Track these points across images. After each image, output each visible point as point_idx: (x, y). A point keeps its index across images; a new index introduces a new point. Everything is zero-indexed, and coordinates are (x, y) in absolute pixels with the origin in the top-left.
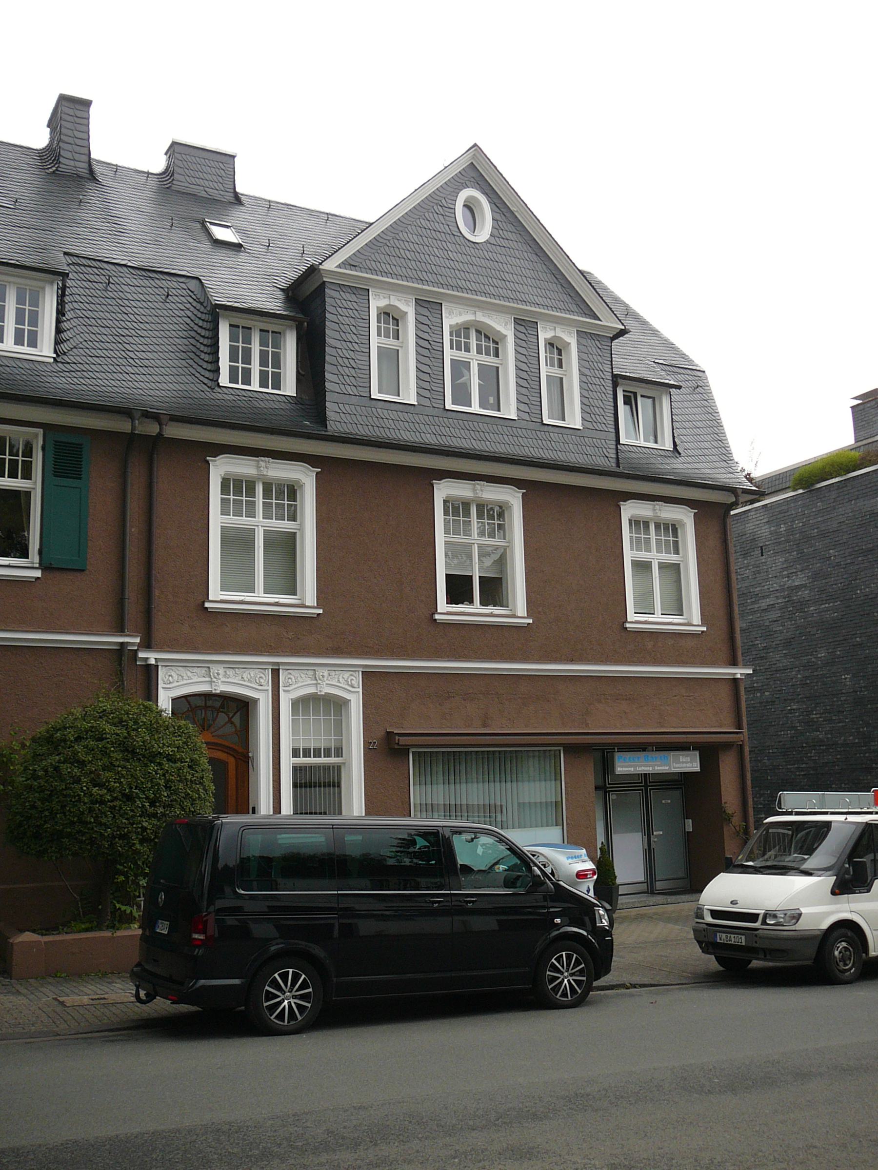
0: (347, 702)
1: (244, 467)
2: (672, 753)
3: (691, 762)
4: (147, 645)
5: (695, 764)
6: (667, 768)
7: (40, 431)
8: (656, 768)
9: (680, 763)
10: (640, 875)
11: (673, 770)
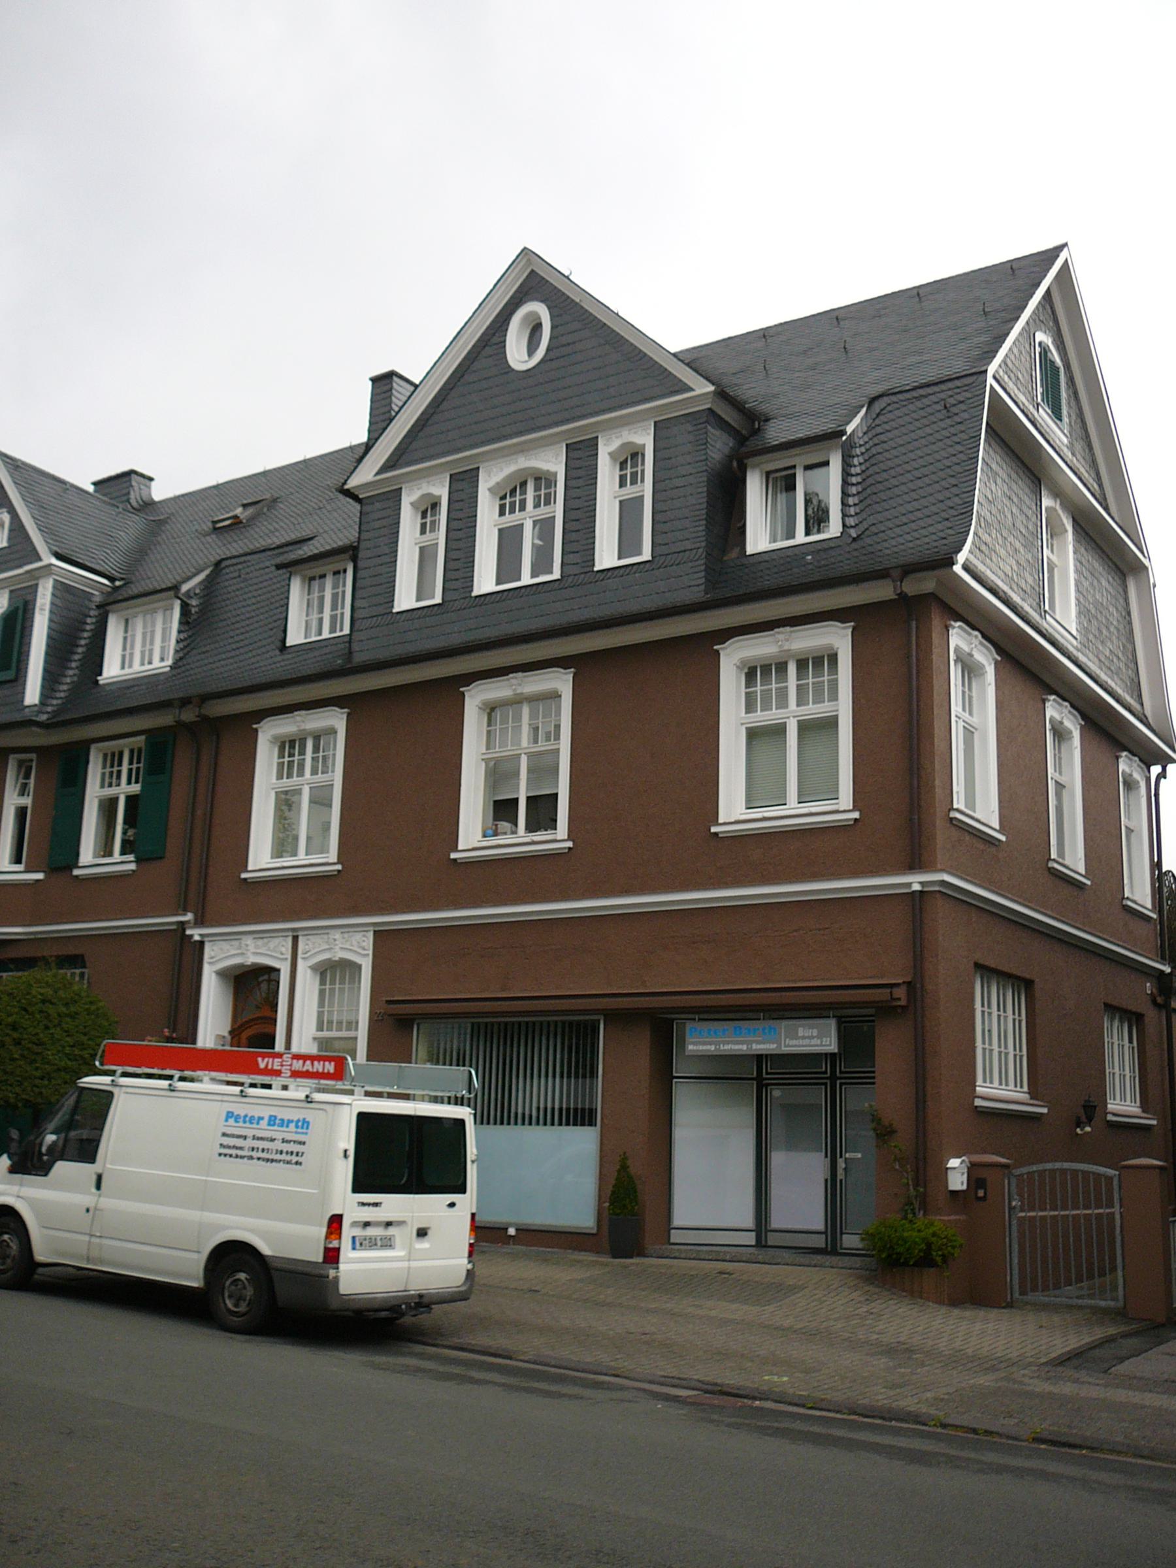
0: (278, 970)
1: (761, 647)
2: (784, 1023)
3: (817, 1037)
4: (200, 922)
5: (826, 1041)
6: (774, 1046)
7: (34, 756)
8: (754, 1046)
9: (797, 1038)
10: (815, 1219)
11: (785, 1050)
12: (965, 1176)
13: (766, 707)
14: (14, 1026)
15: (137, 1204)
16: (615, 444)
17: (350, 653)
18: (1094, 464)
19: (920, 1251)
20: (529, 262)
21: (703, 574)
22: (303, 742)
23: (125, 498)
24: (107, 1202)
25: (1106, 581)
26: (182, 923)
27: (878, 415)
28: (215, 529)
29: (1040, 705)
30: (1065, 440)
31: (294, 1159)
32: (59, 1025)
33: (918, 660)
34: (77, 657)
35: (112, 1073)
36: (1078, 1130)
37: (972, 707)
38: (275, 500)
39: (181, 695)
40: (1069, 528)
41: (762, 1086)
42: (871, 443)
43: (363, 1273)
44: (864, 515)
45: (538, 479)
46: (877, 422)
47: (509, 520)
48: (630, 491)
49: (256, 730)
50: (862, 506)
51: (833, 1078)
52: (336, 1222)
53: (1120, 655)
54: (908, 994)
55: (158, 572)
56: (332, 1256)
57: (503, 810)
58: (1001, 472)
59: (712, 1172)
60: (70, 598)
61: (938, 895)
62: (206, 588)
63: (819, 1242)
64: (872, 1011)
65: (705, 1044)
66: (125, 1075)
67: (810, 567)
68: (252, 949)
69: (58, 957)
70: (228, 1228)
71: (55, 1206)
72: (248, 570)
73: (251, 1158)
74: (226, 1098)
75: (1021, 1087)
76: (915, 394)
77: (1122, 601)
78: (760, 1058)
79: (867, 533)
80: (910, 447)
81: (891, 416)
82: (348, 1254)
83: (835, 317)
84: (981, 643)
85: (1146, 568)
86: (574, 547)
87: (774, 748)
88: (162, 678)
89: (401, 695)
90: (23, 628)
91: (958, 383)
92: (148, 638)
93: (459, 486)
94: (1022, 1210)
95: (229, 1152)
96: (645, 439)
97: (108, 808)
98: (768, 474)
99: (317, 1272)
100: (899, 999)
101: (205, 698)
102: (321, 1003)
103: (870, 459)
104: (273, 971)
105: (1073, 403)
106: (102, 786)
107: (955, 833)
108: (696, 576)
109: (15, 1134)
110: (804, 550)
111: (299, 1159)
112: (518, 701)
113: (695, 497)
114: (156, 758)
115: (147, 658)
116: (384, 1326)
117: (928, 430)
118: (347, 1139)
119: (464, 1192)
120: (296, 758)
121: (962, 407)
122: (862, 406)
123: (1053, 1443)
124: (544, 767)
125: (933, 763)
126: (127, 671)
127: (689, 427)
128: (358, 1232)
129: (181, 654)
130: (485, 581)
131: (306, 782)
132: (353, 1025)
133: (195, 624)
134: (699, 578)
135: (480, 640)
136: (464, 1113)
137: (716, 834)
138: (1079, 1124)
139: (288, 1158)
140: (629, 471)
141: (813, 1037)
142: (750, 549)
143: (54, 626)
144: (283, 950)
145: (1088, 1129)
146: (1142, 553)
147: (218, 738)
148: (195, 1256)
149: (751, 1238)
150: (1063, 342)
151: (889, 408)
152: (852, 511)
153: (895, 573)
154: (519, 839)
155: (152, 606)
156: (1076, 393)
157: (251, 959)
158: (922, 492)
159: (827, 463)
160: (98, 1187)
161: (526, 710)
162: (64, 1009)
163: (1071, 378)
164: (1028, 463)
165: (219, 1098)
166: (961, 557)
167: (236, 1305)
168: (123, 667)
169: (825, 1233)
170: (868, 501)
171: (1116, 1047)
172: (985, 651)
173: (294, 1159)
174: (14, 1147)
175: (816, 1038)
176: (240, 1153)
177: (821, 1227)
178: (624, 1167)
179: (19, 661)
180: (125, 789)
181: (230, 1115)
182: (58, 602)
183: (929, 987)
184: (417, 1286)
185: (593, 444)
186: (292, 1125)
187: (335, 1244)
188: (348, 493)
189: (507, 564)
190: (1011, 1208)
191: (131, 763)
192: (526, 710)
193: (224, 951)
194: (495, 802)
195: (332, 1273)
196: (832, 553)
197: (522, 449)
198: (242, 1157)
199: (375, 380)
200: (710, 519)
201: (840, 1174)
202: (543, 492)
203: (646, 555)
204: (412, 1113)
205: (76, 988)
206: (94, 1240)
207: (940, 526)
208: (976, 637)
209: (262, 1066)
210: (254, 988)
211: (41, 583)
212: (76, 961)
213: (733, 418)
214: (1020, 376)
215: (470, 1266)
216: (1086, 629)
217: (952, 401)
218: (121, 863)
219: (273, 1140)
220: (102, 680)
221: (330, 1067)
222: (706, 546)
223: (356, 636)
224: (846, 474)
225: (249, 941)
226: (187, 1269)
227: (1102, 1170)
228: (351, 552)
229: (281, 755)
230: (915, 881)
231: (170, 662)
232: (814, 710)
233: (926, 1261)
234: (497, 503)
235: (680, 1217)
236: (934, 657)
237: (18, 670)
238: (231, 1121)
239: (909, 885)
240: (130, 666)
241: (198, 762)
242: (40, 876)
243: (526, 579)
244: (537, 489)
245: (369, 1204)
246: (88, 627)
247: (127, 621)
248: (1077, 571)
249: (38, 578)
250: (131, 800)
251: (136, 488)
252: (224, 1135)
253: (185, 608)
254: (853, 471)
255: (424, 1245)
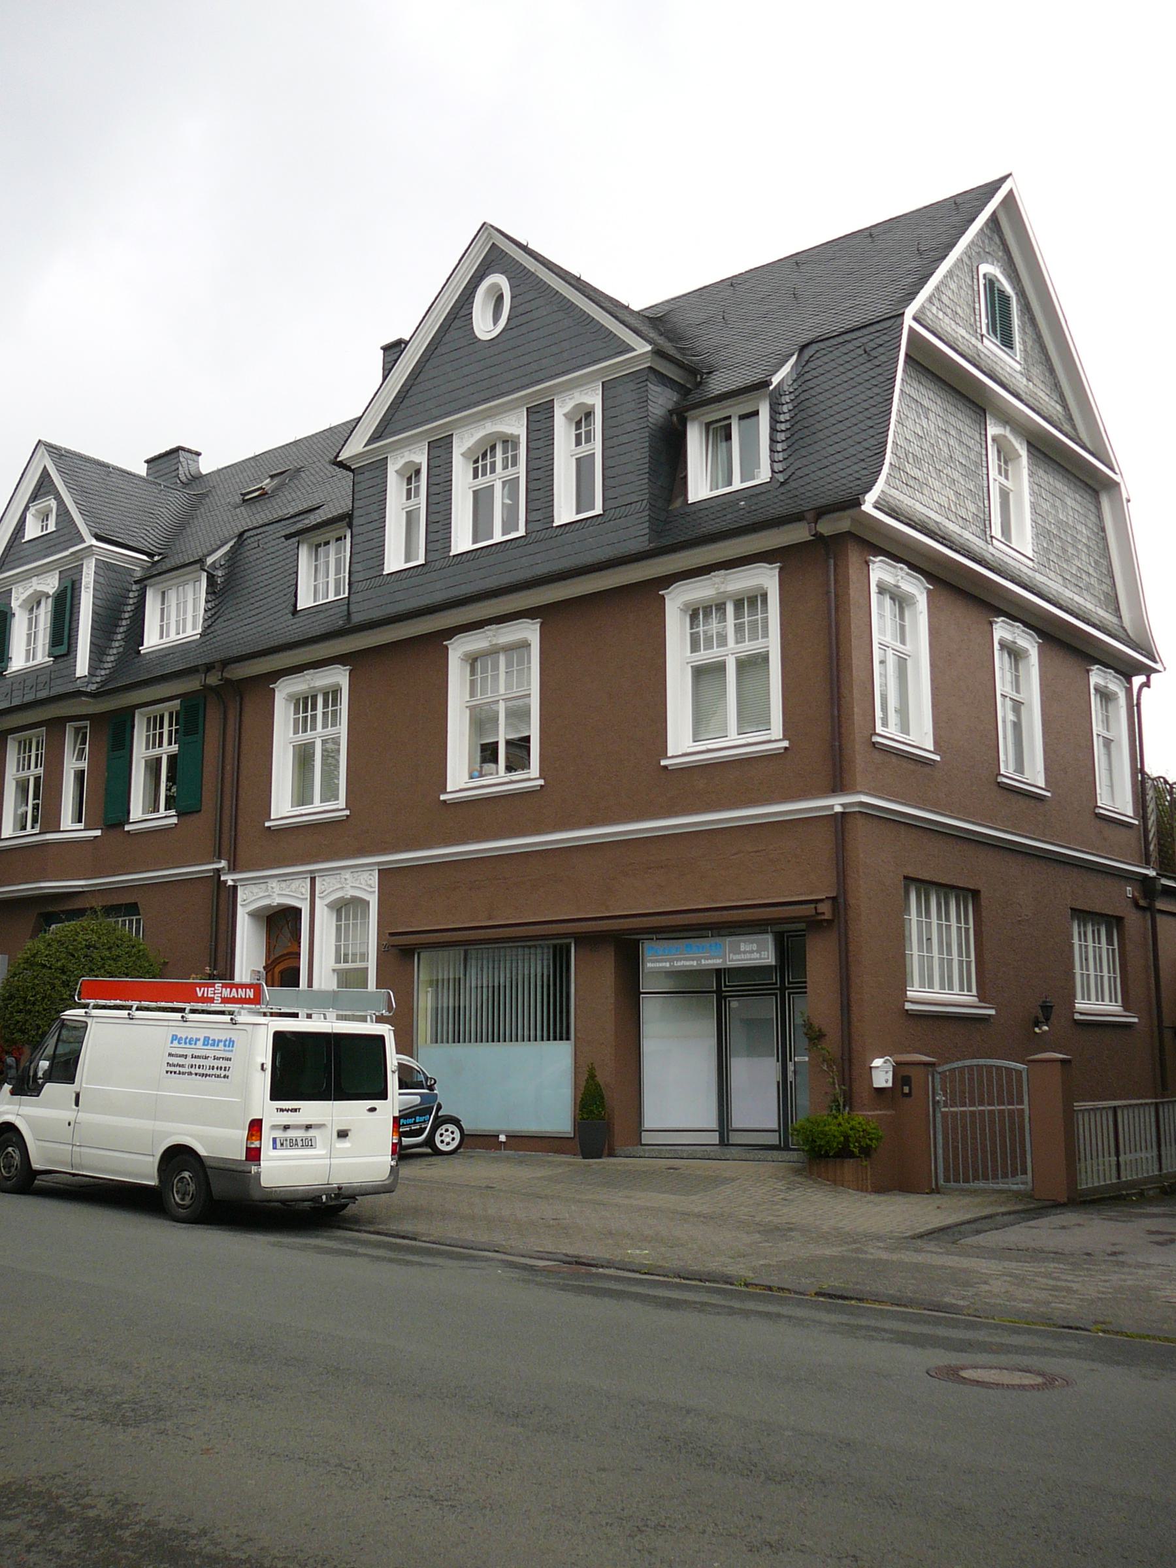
2: (728, 939)
3: (757, 951)
4: (233, 868)
5: (764, 954)
6: (719, 961)
8: (703, 962)
9: (740, 952)
11: (730, 964)
12: (891, 1073)
13: (709, 646)
14: (63, 971)
15: (115, 1118)
16: (568, 408)
17: (349, 614)
18: (1057, 386)
19: (839, 1143)
20: (490, 236)
21: (647, 524)
22: (314, 698)
23: (174, 474)
24: (84, 1116)
25: (1072, 502)
26: (218, 870)
27: (807, 362)
28: (244, 501)
29: (987, 627)
30: (1018, 367)
31: (223, 1073)
32: (103, 967)
33: (836, 595)
34: (122, 630)
35: (86, 1006)
36: (1037, 1030)
37: (899, 636)
38: (298, 470)
39: (207, 661)
40: (1023, 452)
41: (721, 998)
42: (800, 390)
43: (283, 1169)
44: (791, 460)
45: (505, 442)
46: (806, 369)
47: (482, 482)
48: (584, 449)
49: (273, 690)
50: (789, 452)
51: (783, 989)
52: (256, 1126)
53: (1091, 571)
54: (834, 910)
55: (191, 548)
56: (254, 1155)
57: (489, 753)
58: (933, 407)
59: (678, 1078)
60: (112, 575)
61: (858, 816)
62: (230, 559)
63: (773, 1139)
64: (802, 926)
65: (686, 959)
66: (96, 1007)
67: (742, 512)
68: (277, 891)
69: (104, 907)
70: (174, 1134)
71: (44, 1121)
72: (266, 540)
73: (190, 1074)
74: (171, 1023)
75: (970, 990)
76: (840, 340)
77: (1093, 518)
78: (718, 971)
79: (794, 477)
80: (834, 392)
81: (819, 363)
82: (267, 1152)
83: (796, 261)
84: (908, 574)
85: (1118, 484)
86: (537, 505)
87: (714, 684)
88: (193, 645)
89: (393, 651)
90: (72, 606)
91: (878, 327)
92: (181, 607)
93: (436, 452)
94: (945, 1106)
95: (174, 1070)
96: (594, 398)
97: (153, 766)
98: (708, 425)
99: (240, 1168)
100: (823, 914)
101: (225, 663)
102: (338, 939)
103: (799, 406)
104: (298, 911)
105: (1029, 330)
106: (147, 748)
107: (878, 757)
108: (641, 527)
109: (10, 1060)
110: (738, 496)
111: (227, 1073)
112: (494, 651)
113: (638, 454)
114: (189, 722)
115: (181, 626)
116: (319, 1214)
117: (850, 374)
118: (264, 1053)
119: (386, 1098)
120: (309, 713)
121: (881, 350)
122: (792, 355)
123: (830, 1296)
124: (519, 715)
125: (851, 692)
126: (165, 640)
127: (632, 386)
128: (279, 1134)
129: (209, 622)
130: (462, 541)
131: (318, 735)
132: (364, 957)
133: (221, 593)
134: (644, 528)
135: (462, 596)
136: (385, 1030)
137: (665, 767)
138: (1037, 1023)
139: (218, 1072)
140: (583, 430)
141: (752, 952)
142: (692, 499)
143: (98, 602)
144: (303, 890)
145: (1046, 1028)
146: (1112, 469)
147: (242, 699)
148: (151, 1159)
149: (715, 1138)
150: (1015, 270)
151: (818, 355)
152: (780, 456)
153: (810, 516)
154: (499, 779)
155: (182, 579)
156: (1033, 320)
157: (277, 900)
158: (842, 435)
159: (756, 413)
160: (77, 1104)
161: (502, 659)
162: (107, 953)
163: (1021, 305)
164: (968, 396)
165: (166, 1023)
166: (870, 498)
167: (183, 1199)
168: (161, 637)
169: (779, 1131)
170: (796, 446)
171: (1090, 950)
172: (914, 581)
173: (222, 1073)
174: (12, 1073)
175: (756, 952)
176: (182, 1070)
177: (775, 1126)
178: (592, 1076)
179: (70, 637)
180: (169, 749)
181: (174, 1038)
182: (101, 580)
183: (852, 901)
184: (341, 1178)
185: (549, 407)
186: (221, 1044)
187: (256, 1144)
188: (341, 465)
189: (481, 526)
190: (936, 1103)
191: (170, 725)
192: (502, 659)
193: (256, 894)
194: (482, 745)
195: (254, 1169)
196: (762, 498)
197: (489, 415)
198: (184, 1073)
199: (386, 349)
200: (653, 473)
201: (790, 1077)
202: (510, 454)
203: (598, 510)
204: (329, 1031)
205: (118, 933)
206: (75, 1148)
207: (856, 468)
208: (901, 569)
209: (200, 995)
210: (282, 924)
211: (85, 562)
212: (132, 909)
213: (678, 368)
214: (959, 311)
215: (393, 1163)
216: (1046, 550)
217: (872, 345)
218: (166, 817)
219: (206, 1058)
220: (143, 650)
221: (250, 993)
222: (650, 498)
223: (353, 598)
224: (774, 421)
225: (273, 883)
226: (143, 1170)
227: (1013, 1064)
228: (347, 519)
229: (297, 712)
230: (837, 803)
231: (199, 630)
232: (750, 647)
233: (844, 1153)
234: (472, 466)
235: (652, 1118)
236: (852, 592)
237: (69, 645)
238: (176, 1042)
239: (832, 807)
240: (168, 636)
241: (225, 719)
242: (98, 833)
243: (498, 537)
244: (505, 452)
245: (287, 1110)
246: (131, 601)
247: (163, 593)
248: (1033, 493)
249: (82, 559)
250: (172, 759)
251: (184, 464)
252: (170, 1055)
253: (211, 579)
254: (782, 418)
255: (345, 1144)
